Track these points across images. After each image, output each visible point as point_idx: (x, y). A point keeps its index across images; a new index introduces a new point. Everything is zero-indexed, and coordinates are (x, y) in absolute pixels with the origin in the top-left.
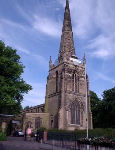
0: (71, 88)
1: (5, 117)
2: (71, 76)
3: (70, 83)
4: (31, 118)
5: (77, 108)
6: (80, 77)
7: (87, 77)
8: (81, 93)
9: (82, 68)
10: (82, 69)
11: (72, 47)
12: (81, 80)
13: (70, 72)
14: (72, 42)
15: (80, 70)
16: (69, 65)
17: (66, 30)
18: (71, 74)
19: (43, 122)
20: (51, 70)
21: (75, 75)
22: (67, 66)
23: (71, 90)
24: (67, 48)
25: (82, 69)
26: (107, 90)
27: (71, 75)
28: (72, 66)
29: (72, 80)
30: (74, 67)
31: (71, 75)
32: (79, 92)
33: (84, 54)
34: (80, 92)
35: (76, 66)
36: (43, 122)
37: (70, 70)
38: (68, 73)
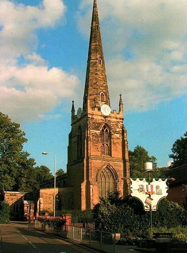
0: (99, 151)
1: (16, 196)
2: (98, 134)
3: (96, 145)
4: (47, 197)
5: (95, 164)
6: (113, 133)
7: (123, 132)
8: (115, 157)
9: (116, 118)
10: (117, 120)
11: (102, 86)
12: (115, 137)
13: (97, 128)
14: (101, 77)
15: (114, 122)
16: (95, 117)
17: (93, 58)
18: (99, 130)
19: (65, 200)
20: (74, 123)
21: (107, 131)
22: (92, 118)
23: (99, 153)
24: (94, 88)
25: (117, 120)
26: (141, 147)
27: (98, 132)
28: (100, 118)
29: (88, 135)
30: (103, 118)
31: (98, 132)
32: (111, 156)
33: (120, 95)
34: (112, 156)
35: (106, 117)
36: (65, 200)
37: (97, 125)
38: (93, 129)
